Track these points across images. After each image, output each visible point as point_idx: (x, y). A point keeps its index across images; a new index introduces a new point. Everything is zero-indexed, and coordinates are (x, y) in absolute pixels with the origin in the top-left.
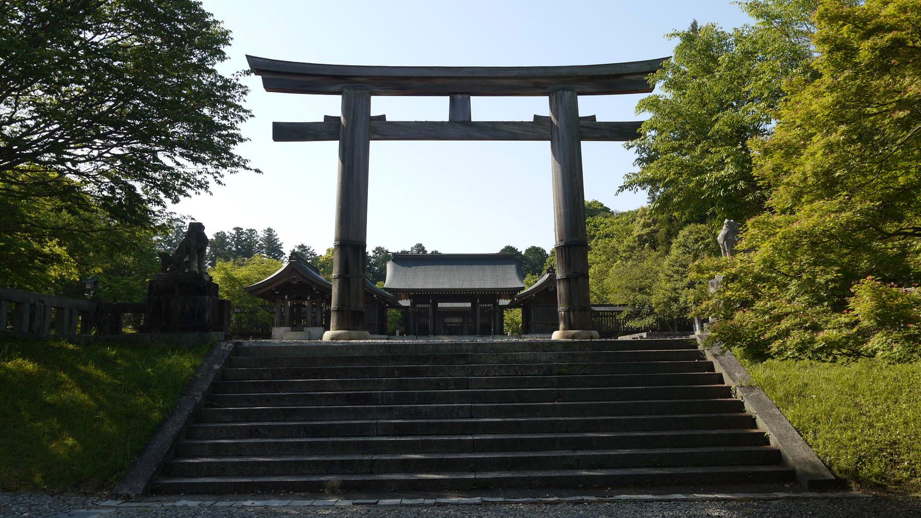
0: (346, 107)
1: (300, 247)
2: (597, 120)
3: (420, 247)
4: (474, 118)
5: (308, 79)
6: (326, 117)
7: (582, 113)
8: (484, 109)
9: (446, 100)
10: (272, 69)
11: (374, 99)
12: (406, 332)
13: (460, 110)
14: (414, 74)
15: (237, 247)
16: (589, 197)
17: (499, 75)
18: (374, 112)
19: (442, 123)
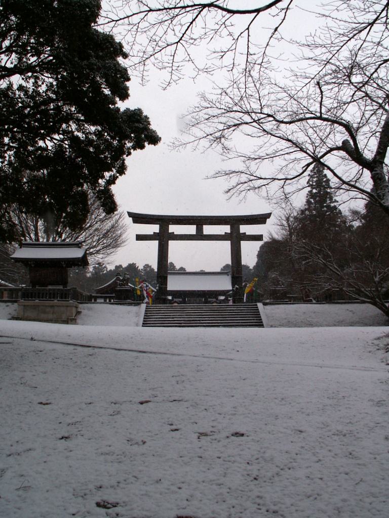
0: (231, 228)
6: (154, 233)
7: (170, 231)
8: (208, 230)
9: (195, 227)
11: (241, 226)
13: (200, 229)
16: (243, 263)
19: (194, 235)
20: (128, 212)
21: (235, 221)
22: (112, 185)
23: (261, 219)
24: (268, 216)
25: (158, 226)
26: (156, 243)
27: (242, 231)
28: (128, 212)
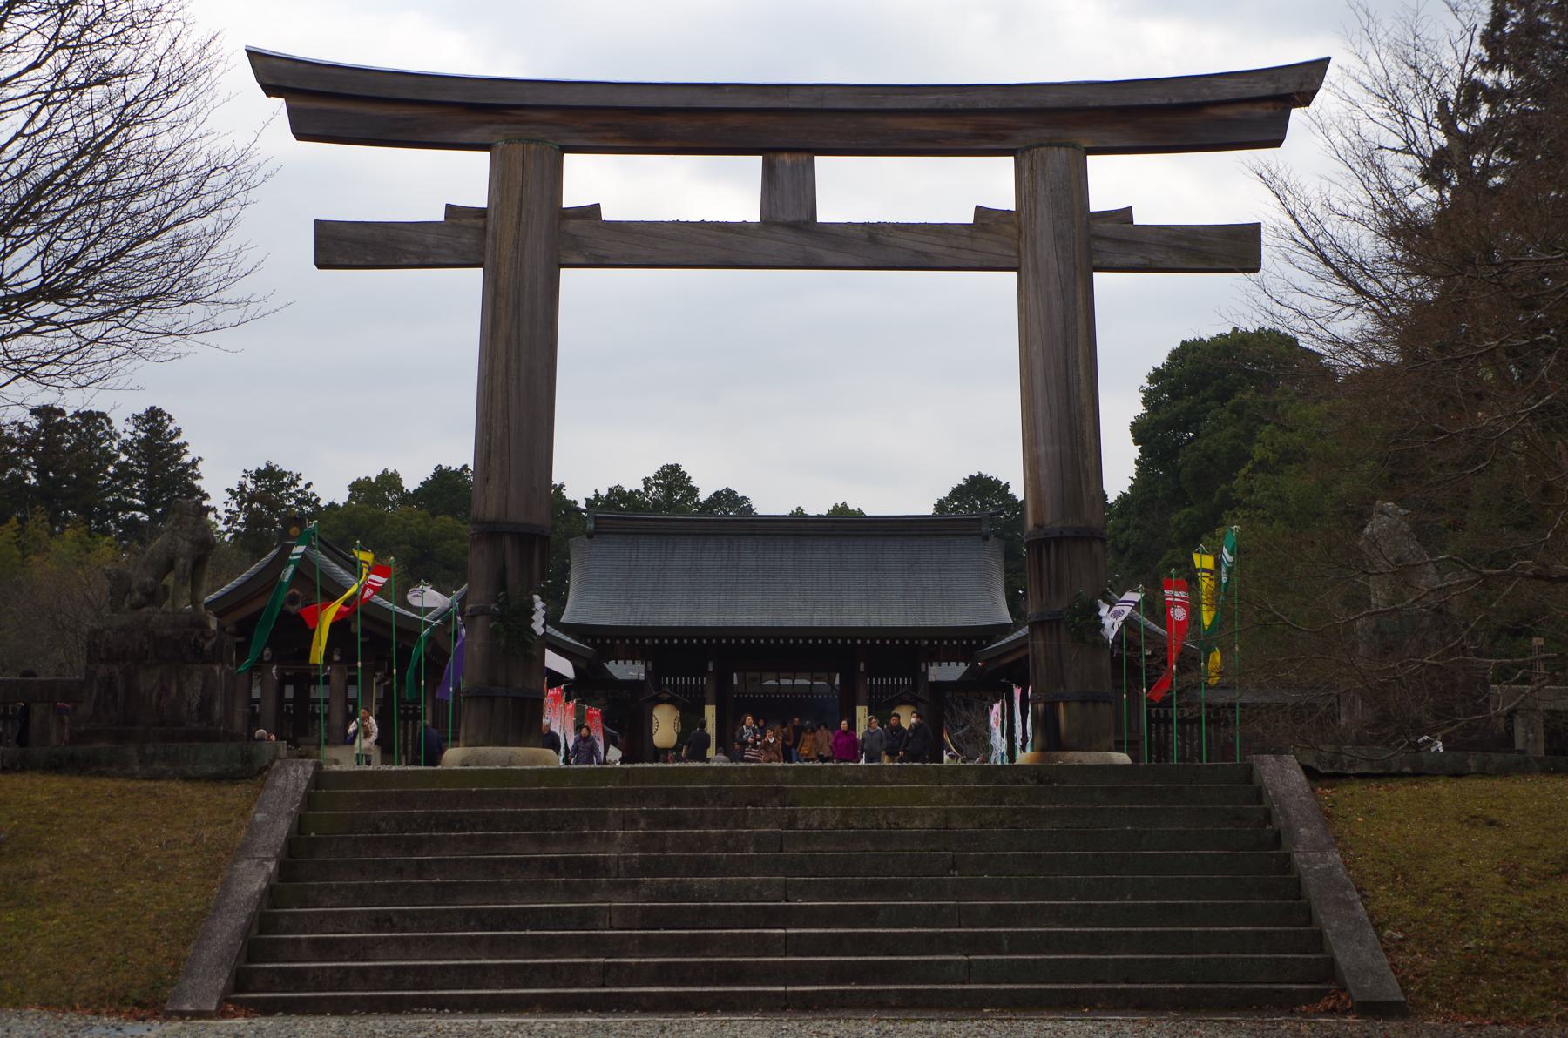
0: (499, 180)
1: (260, 475)
2: (1137, 221)
3: (673, 477)
4: (823, 216)
5: (406, 112)
6: (450, 208)
7: (1097, 203)
8: (851, 189)
10: (315, 86)
11: (571, 161)
12: (299, 940)
13: (788, 197)
14: (671, 101)
15: (41, 474)
17: (888, 105)
18: (572, 197)
19: (742, 228)
20: (253, 55)
21: (1051, 125)
22: (569, 494)
23: (1240, 111)
24: (1298, 84)
25: (480, 161)
26: (464, 287)
27: (1099, 201)
28: (253, 55)
